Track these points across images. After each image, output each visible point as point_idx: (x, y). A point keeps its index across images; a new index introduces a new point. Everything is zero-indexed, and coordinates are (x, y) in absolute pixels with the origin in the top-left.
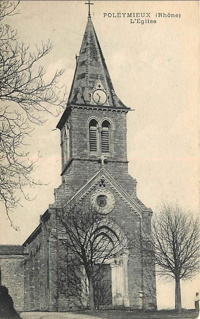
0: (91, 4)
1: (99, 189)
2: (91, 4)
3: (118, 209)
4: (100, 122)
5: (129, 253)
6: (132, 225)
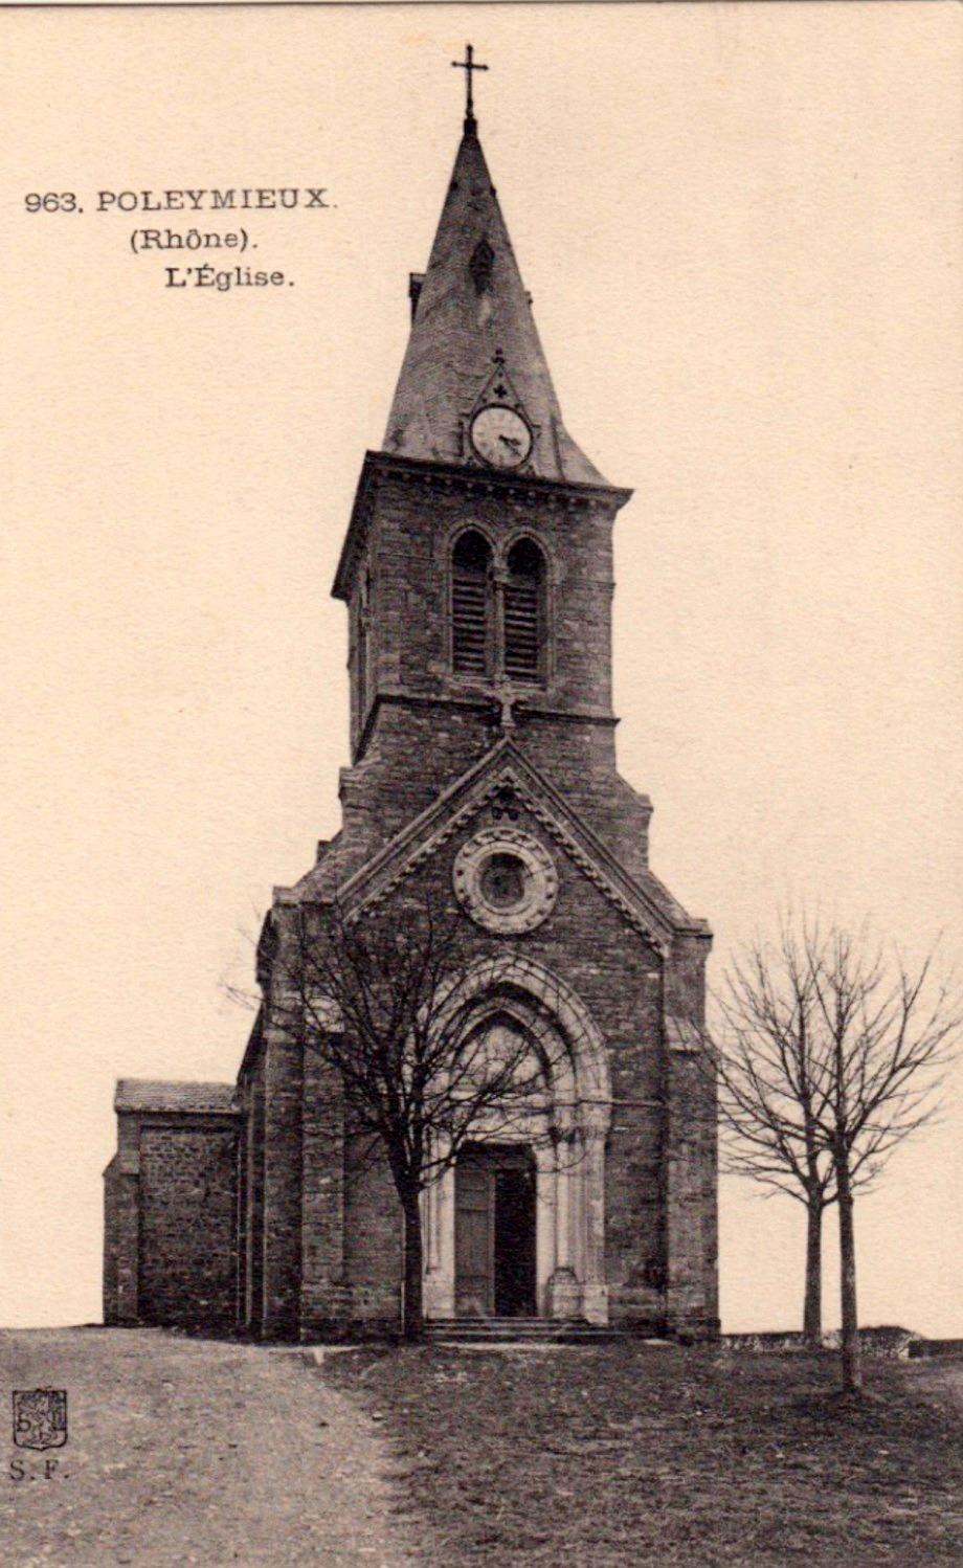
0: (478, 67)
1: (490, 826)
2: (478, 67)
3: (570, 914)
4: (500, 546)
5: (611, 1100)
6: (626, 985)
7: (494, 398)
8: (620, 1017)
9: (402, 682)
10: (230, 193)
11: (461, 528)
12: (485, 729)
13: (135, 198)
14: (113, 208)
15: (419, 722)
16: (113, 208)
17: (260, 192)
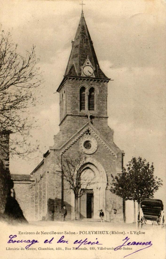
7: (87, 64)
8: (108, 168)
9: (71, 112)
10: (97, 232)
11: (81, 86)
12: (85, 119)
13: (85, 233)
14: (81, 234)
15: (74, 119)
16: (81, 234)
17: (100, 232)
